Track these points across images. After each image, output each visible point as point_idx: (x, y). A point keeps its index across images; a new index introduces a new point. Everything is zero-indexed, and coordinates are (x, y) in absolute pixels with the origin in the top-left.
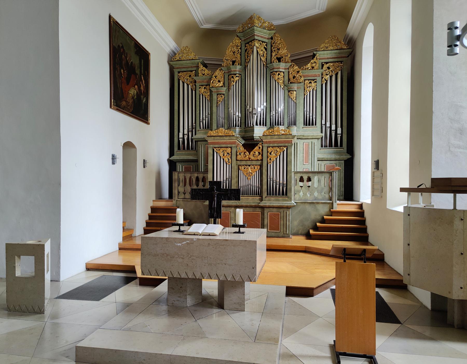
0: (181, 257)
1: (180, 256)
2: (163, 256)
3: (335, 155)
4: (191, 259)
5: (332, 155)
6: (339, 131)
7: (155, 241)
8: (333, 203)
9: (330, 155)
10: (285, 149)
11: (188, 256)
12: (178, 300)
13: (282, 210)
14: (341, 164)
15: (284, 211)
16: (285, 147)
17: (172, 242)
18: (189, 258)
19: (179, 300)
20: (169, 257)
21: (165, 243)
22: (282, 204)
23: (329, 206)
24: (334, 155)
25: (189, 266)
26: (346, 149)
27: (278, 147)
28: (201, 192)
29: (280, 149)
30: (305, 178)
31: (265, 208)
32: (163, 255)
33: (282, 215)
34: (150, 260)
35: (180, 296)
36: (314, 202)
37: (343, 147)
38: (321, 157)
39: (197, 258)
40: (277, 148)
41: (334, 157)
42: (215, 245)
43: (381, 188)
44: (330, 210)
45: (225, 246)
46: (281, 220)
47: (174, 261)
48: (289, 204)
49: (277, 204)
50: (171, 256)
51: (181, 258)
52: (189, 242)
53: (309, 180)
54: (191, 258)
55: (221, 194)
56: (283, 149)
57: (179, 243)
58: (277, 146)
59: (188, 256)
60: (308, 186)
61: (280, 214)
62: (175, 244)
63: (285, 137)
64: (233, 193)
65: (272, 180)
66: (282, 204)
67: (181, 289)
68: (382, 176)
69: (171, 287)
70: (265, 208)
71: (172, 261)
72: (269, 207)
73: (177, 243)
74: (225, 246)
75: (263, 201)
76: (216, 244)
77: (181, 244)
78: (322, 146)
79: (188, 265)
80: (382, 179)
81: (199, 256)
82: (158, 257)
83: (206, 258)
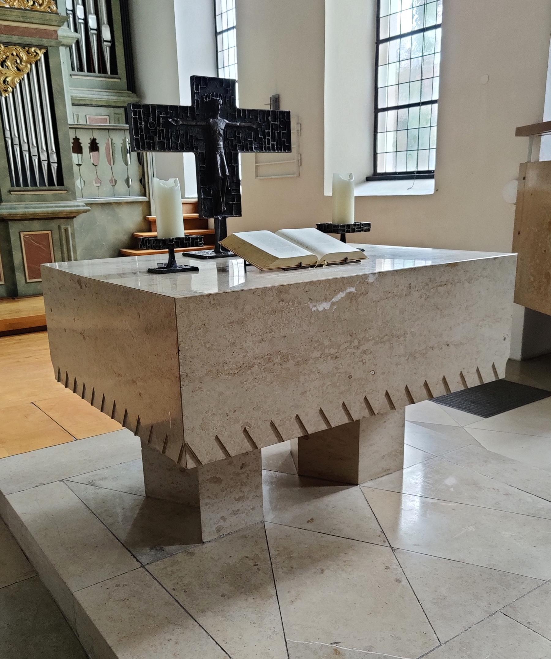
0: (330, 354)
1: (327, 351)
2: (268, 365)
3: (107, 94)
4: (361, 353)
5: (101, 93)
6: (106, 34)
7: (236, 308)
8: (149, 203)
9: (97, 93)
10: (42, 56)
11: (351, 342)
12: (235, 513)
13: (54, 224)
14: (119, 116)
15: (59, 227)
16: (40, 47)
17: (299, 303)
18: (354, 350)
19: (238, 510)
20: (290, 364)
21: (274, 311)
22: (56, 207)
23: (141, 208)
24: (104, 93)
25: (354, 379)
26: (124, 80)
27: (23, 46)
28: (170, 120)
29: (29, 53)
30: (85, 144)
31: (10, 222)
32: (270, 360)
33: (56, 236)
34: (221, 394)
35: (241, 494)
36: (112, 202)
37: (119, 74)
38: (78, 95)
39: (376, 343)
40: (19, 48)
41: (106, 97)
42: (426, 287)
43: (300, 155)
44: (145, 219)
45: (449, 286)
46: (55, 248)
47: (307, 376)
48: (74, 206)
49: (44, 207)
50: (299, 359)
51: (332, 358)
52: (353, 290)
53: (94, 146)
54: (360, 350)
55: (237, 126)
56: (37, 53)
57: (322, 301)
58: (19, 45)
59: (353, 345)
60: (77, 165)
61: (50, 236)
62: (311, 307)
63: (42, 19)
64: (272, 124)
65: (16, 141)
66: (56, 207)
67: (244, 470)
68: (299, 129)
69: (209, 477)
70: (10, 222)
71: (302, 379)
72: (24, 218)
73: (317, 301)
74: (449, 286)
75: (2, 202)
76: (427, 284)
77: (329, 304)
78: (73, 69)
79: (350, 377)
80: (301, 135)
81: (384, 337)
82: (252, 374)
83: (402, 338)
